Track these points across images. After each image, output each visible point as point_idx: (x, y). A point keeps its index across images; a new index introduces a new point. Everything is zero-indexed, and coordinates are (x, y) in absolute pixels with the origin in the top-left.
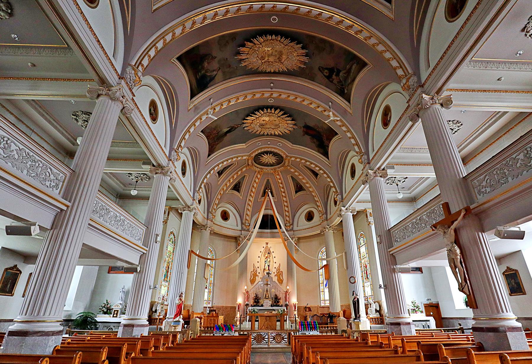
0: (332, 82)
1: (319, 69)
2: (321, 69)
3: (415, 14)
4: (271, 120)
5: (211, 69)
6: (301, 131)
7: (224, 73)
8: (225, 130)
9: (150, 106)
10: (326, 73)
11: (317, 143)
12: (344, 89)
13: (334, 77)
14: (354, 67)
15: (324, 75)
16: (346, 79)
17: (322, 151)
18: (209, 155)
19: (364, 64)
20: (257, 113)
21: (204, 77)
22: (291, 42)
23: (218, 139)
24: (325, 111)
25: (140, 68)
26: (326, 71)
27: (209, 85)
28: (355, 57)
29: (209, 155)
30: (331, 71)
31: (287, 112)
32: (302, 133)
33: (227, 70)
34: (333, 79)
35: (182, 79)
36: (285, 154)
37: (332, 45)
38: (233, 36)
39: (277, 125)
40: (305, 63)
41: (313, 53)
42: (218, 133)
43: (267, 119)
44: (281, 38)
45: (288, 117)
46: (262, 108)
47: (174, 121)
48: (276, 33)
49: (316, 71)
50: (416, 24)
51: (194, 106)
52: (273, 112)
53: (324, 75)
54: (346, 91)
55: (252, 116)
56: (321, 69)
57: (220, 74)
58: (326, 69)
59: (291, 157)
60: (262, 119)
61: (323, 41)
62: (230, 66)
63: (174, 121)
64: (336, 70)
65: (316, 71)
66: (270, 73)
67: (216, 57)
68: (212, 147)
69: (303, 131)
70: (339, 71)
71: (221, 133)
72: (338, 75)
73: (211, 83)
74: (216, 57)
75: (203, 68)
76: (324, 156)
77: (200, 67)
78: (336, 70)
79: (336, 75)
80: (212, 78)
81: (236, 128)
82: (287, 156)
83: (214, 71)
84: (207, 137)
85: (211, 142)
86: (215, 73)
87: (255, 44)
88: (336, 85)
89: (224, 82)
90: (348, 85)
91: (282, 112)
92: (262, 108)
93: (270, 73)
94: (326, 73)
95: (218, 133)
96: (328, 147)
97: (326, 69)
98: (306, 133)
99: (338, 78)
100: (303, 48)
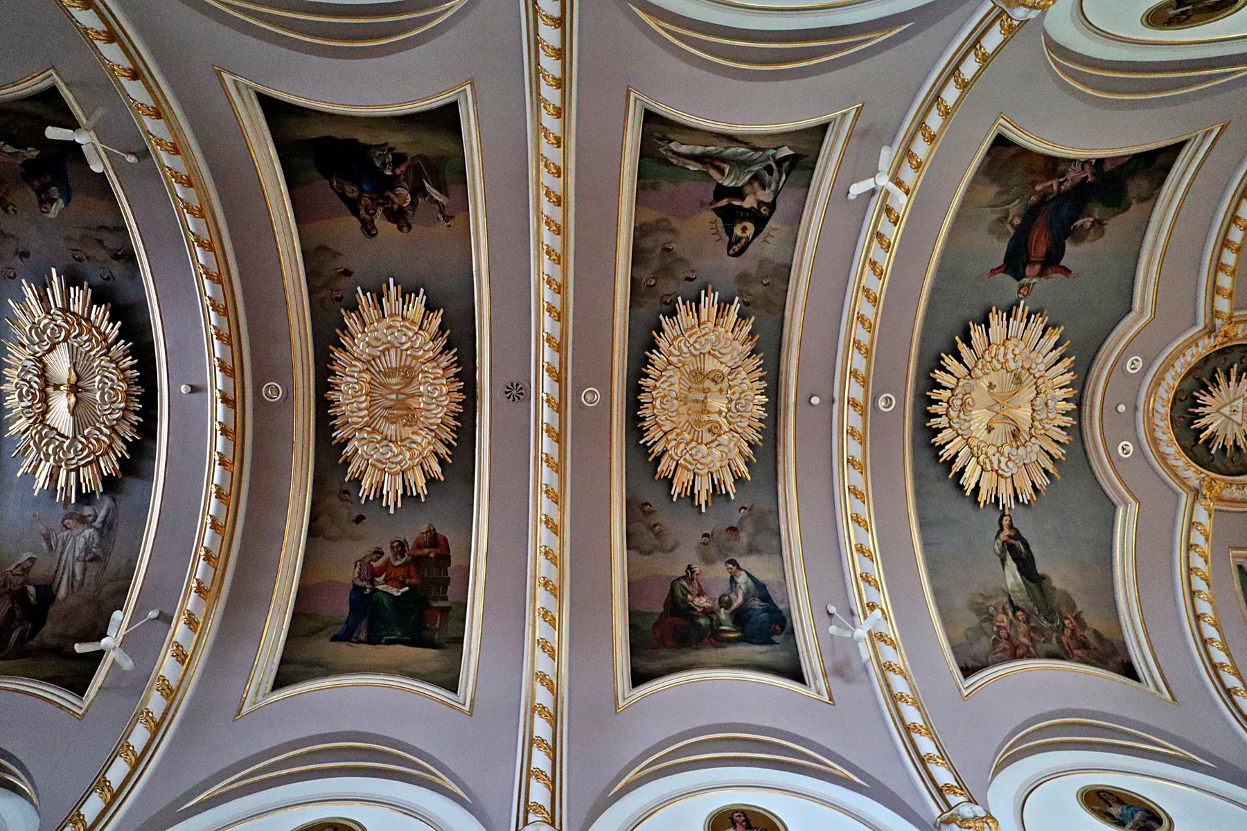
0: (772, 207)
1: (737, 254)
2: (738, 248)
3: (825, 43)
4: (989, 401)
5: (725, 587)
6: (1044, 286)
7: (752, 550)
8: (1012, 576)
9: (1106, 816)
10: (744, 229)
11: (1097, 211)
12: (779, 163)
13: (749, 203)
14: (684, 149)
15: (756, 235)
16: (740, 164)
17: (1137, 186)
18: (1129, 671)
19: (650, 117)
20: (946, 454)
21: (740, 617)
22: (658, 348)
23: (1050, 613)
24: (889, 211)
25: (953, 799)
26: (738, 231)
27: (781, 607)
28: (647, 152)
29: (1129, 671)
30: (730, 216)
31: (948, 340)
32: (1056, 277)
33: (744, 538)
34: (761, 203)
35: (720, 688)
36: (1194, 342)
37: (641, 231)
38: (636, 510)
39: (1018, 380)
40: (725, 303)
41: (688, 279)
42: (1015, 609)
43: (979, 419)
44: (647, 376)
45: (967, 340)
46: (926, 433)
47: (840, 770)
48: (634, 391)
49: (746, 263)
50: (446, 11)
51: (825, 676)
52: (945, 394)
53: (756, 235)
54: (786, 151)
55: (962, 471)
56: (738, 248)
57: (751, 563)
58: (730, 232)
59: (1215, 314)
60: (982, 434)
61: (638, 256)
62: (733, 529)
63: (840, 770)
64: (724, 202)
65: (746, 263)
66: (774, 408)
67: (689, 567)
68: (1084, 645)
69: (1041, 274)
70: (721, 192)
71: (1021, 598)
72: (738, 193)
73: (776, 597)
74: (689, 567)
75: (708, 612)
76: (1167, 169)
77: (702, 621)
78: (724, 202)
79: (743, 198)
80: (760, 589)
81: (1017, 536)
82: (1211, 330)
83: (733, 580)
84: (1014, 657)
85: (1053, 646)
86: (742, 579)
87: (664, 452)
88: (777, 193)
89: (786, 553)
90: (756, 149)
91: (950, 362)
92: (926, 433)
93: (774, 408)
94: (744, 229)
95: (1015, 609)
96: (1100, 161)
97: (730, 232)
98: (1052, 262)
99: (748, 189)
100: (673, 313)
